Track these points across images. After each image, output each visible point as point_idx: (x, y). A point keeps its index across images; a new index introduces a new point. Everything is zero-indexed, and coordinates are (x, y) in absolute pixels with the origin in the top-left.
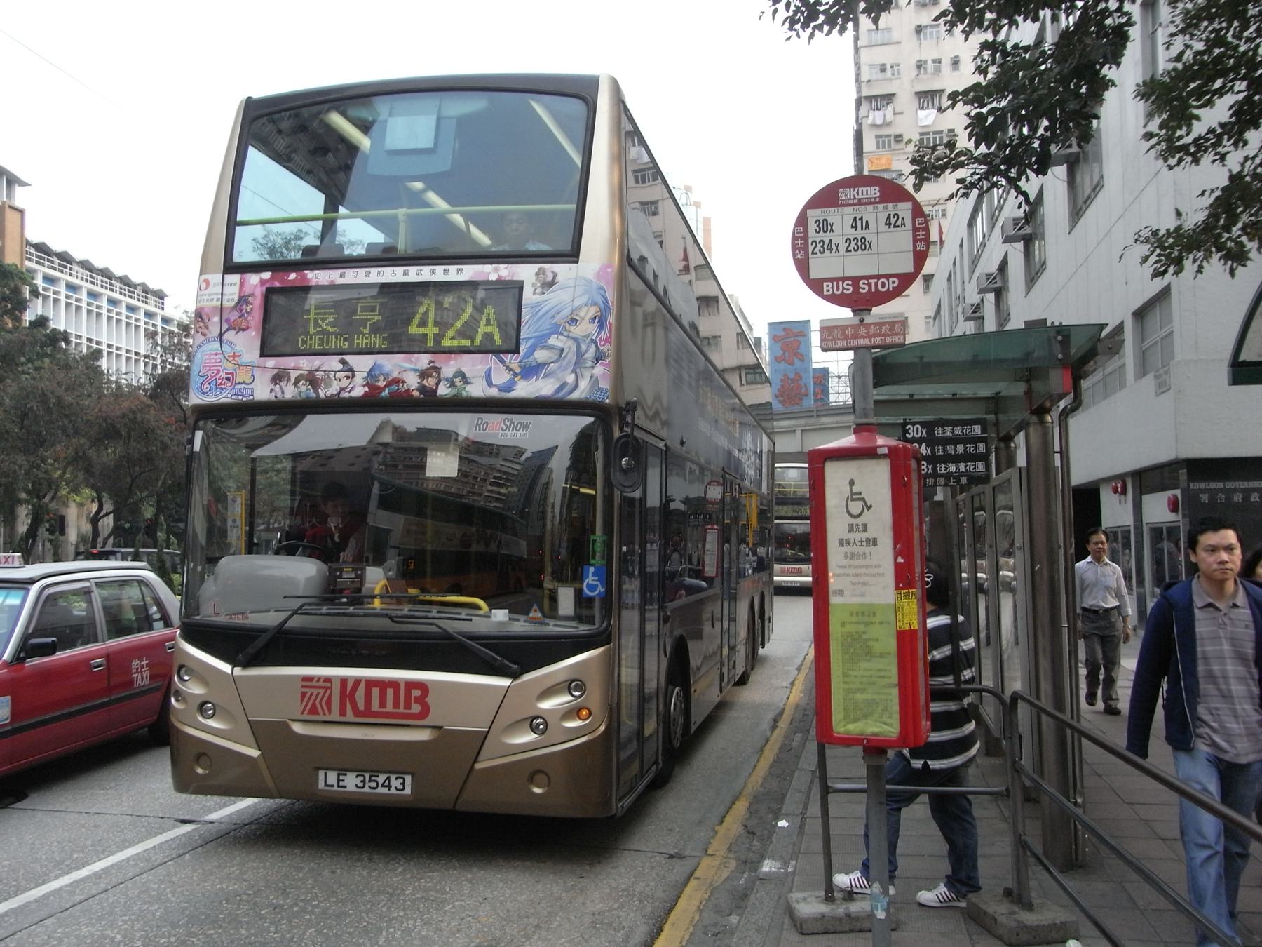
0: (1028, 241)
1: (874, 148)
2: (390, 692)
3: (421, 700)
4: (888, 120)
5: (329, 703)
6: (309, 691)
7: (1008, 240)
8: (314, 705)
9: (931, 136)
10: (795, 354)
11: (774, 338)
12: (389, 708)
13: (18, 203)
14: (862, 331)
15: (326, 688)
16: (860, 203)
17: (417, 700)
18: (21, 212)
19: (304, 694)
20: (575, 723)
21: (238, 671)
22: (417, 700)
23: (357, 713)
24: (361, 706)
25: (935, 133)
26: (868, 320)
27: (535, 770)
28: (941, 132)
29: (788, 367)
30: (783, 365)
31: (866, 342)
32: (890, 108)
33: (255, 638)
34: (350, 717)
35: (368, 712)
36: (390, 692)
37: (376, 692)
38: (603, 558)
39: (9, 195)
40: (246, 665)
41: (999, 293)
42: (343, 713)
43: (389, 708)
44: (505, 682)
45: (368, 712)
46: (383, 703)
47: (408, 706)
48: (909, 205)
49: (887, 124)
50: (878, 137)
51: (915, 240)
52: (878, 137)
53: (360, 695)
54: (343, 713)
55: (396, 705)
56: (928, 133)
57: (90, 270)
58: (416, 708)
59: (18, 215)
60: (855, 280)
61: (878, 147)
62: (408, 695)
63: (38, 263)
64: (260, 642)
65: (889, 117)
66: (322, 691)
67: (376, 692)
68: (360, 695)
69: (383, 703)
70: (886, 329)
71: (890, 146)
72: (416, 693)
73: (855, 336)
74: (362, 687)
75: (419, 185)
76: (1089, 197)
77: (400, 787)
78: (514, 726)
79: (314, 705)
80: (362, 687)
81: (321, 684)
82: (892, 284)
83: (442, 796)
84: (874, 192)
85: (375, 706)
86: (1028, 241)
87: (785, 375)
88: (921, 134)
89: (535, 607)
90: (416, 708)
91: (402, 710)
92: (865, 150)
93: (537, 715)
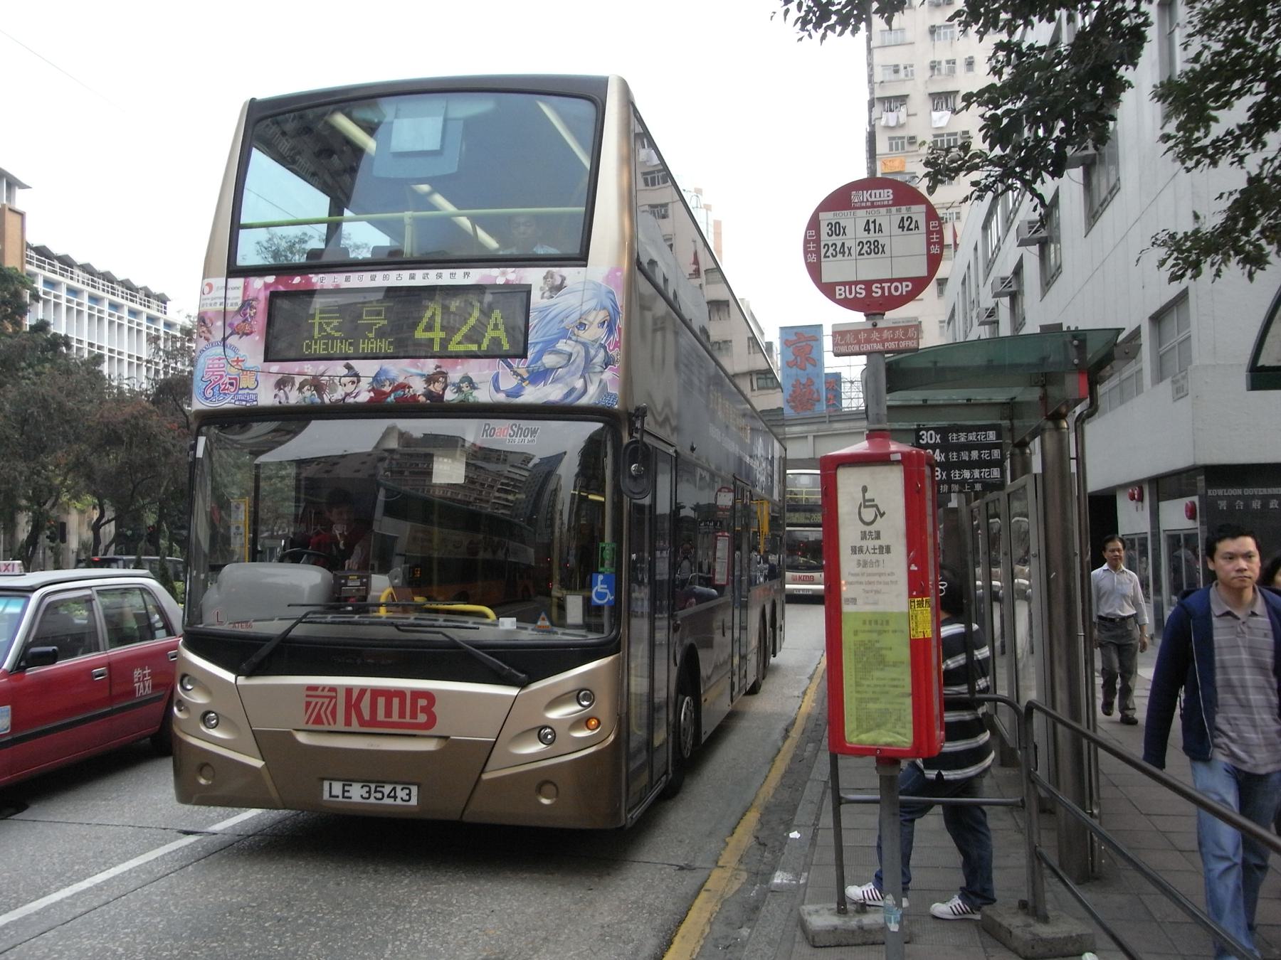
0: (1044, 244)
1: (887, 150)
2: (396, 701)
3: (428, 710)
4: (902, 121)
5: (334, 713)
6: (314, 700)
7: (1023, 243)
8: (319, 714)
9: (945, 138)
10: (807, 359)
11: (786, 343)
12: (395, 717)
13: (18, 206)
14: (875, 335)
15: (331, 698)
16: (873, 205)
17: (423, 710)
18: (22, 215)
19: (308, 704)
20: (584, 733)
21: (242, 680)
22: (423, 710)
23: (362, 722)
24: (367, 716)
25: (949, 135)
26: (881, 324)
27: (543, 780)
28: (955, 134)
29: (800, 372)
30: (794, 370)
31: (879, 347)
32: (903, 109)
33: (259, 647)
34: (355, 726)
35: (373, 722)
36: (396, 701)
37: (381, 701)
38: (612, 565)
39: (9, 198)
40: (250, 674)
41: (1015, 297)
42: (348, 723)
43: (395, 717)
44: (513, 692)
45: (373, 722)
46: (388, 713)
47: (414, 715)
48: (922, 208)
49: (900, 126)
50: (891, 139)
51: (929, 244)
52: (891, 139)
53: (365, 705)
54: (348, 723)
55: (402, 715)
56: (942, 135)
57: (91, 274)
58: (422, 718)
59: (18, 218)
60: (868, 284)
61: (891, 149)
62: (414, 704)
64: (264, 651)
65: (903, 119)
66: (327, 701)
67: (381, 701)
68: (365, 705)
69: (388, 713)
70: (900, 333)
71: (903, 148)
72: (422, 702)
73: (868, 341)
74: (367, 696)
75: (425, 188)
76: (1105, 200)
77: (406, 798)
78: (522, 736)
79: (319, 714)
80: (367, 696)
81: (326, 693)
82: (905, 288)
83: (449, 807)
84: (887, 194)
85: (381, 716)
86: (1044, 244)
87: (797, 380)
88: (935, 136)
89: (543, 615)
90: (422, 718)
91: (408, 719)
92: (878, 152)
93: (545, 725)
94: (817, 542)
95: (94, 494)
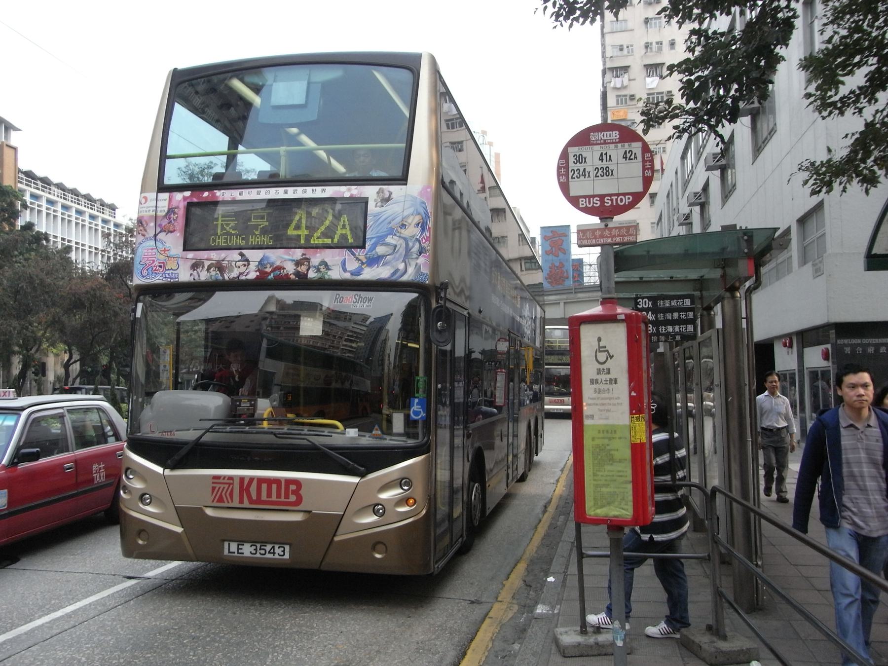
0: (723, 169)
1: (615, 104)
2: (274, 486)
3: (297, 493)
4: (625, 84)
5: (231, 495)
6: (218, 486)
7: (709, 169)
8: (221, 496)
9: (655, 96)
10: (560, 249)
11: (545, 238)
12: (274, 498)
13: (13, 143)
14: (607, 233)
15: (230, 484)
16: (605, 143)
17: (294, 492)
18: (15, 149)
19: (214, 488)
20: (405, 509)
21: (168, 472)
22: (294, 492)
23: (251, 501)
24: (254, 497)
25: (658, 93)
26: (611, 225)
27: (376, 541)
28: (662, 93)
29: (555, 258)
30: (551, 257)
31: (609, 241)
32: (626, 76)
33: (179, 449)
34: (246, 504)
35: (259, 501)
36: (274, 486)
37: (264, 487)
38: (424, 392)
39: (6, 137)
40: (173, 468)
41: (703, 206)
42: (241, 501)
43: (274, 498)
44: (355, 480)
45: (259, 501)
46: (269, 495)
47: (287, 496)
48: (639, 144)
49: (624, 87)
50: (618, 96)
51: (644, 169)
52: (618, 96)
53: (253, 489)
54: (241, 501)
55: (279, 496)
56: (653, 94)
57: (63, 190)
58: (293, 498)
59: (12, 151)
60: (602, 197)
61: (618, 103)
62: (287, 489)
63: (27, 185)
64: (183, 452)
65: (626, 82)
66: (227, 486)
67: (264, 487)
68: (253, 489)
69: (269, 495)
70: (624, 231)
71: (626, 103)
72: (293, 487)
73: (602, 237)
74: (255, 483)
75: (295, 130)
76: (766, 139)
78: (362, 511)
79: (221, 496)
80: (255, 483)
81: (226, 481)
82: (628, 200)
83: (311, 560)
84: (615, 135)
85: (264, 496)
86: (723, 169)
87: (553, 264)
88: (648, 94)
89: (376, 427)
90: (293, 498)
91: (283, 499)
92: (609, 105)
93: (378, 503)
94: (566, 376)
95: (65, 343)
